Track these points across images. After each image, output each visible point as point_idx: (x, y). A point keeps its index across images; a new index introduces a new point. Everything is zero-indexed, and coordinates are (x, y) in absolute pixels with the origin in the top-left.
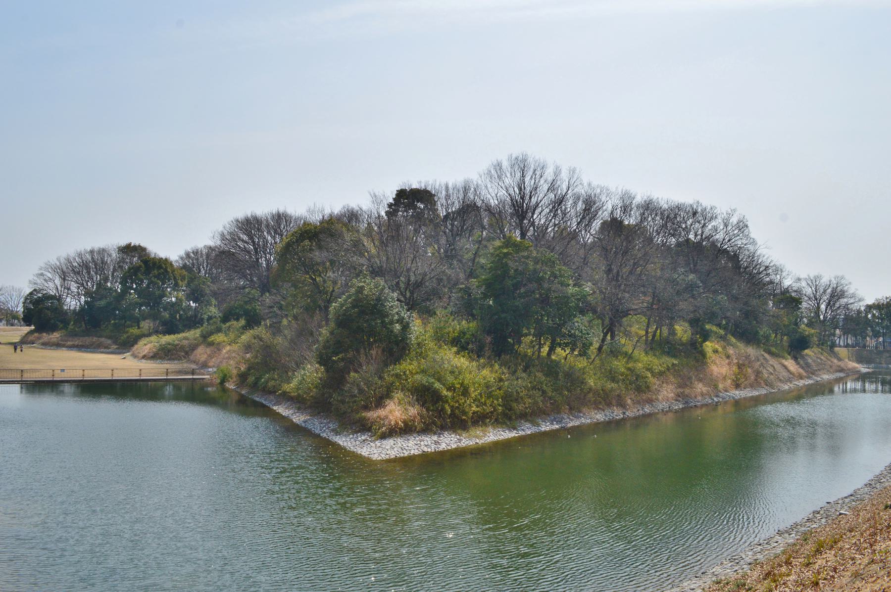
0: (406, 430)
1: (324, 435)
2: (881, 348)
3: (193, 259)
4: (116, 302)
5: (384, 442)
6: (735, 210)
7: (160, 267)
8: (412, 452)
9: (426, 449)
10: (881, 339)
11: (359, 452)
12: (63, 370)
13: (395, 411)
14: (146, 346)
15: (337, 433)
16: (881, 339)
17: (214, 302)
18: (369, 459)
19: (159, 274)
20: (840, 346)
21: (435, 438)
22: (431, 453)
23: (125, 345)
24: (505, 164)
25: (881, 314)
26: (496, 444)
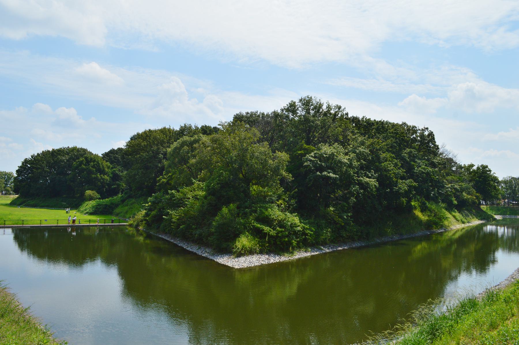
0: (251, 252)
1: (204, 255)
2: (507, 206)
3: (111, 155)
4: (51, 177)
5: (240, 259)
6: (427, 129)
7: (94, 161)
8: (256, 264)
9: (263, 263)
10: (506, 200)
11: (227, 264)
12: (46, 220)
13: (244, 241)
14: (90, 205)
15: (213, 255)
16: (506, 200)
17: (434, 226)
18: (233, 268)
19: (94, 165)
20: (483, 205)
21: (267, 256)
22: (266, 265)
23: (75, 206)
24: (298, 104)
25: (506, 186)
26: (299, 260)
